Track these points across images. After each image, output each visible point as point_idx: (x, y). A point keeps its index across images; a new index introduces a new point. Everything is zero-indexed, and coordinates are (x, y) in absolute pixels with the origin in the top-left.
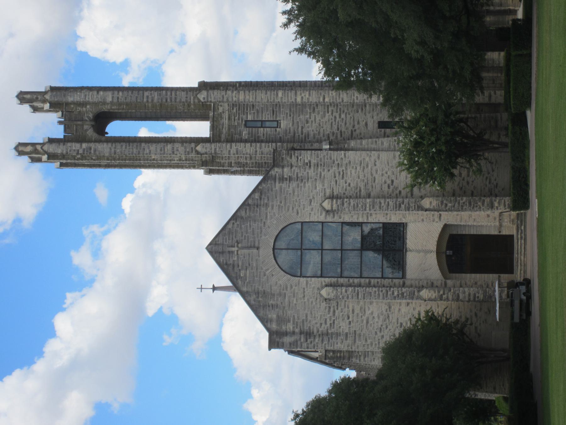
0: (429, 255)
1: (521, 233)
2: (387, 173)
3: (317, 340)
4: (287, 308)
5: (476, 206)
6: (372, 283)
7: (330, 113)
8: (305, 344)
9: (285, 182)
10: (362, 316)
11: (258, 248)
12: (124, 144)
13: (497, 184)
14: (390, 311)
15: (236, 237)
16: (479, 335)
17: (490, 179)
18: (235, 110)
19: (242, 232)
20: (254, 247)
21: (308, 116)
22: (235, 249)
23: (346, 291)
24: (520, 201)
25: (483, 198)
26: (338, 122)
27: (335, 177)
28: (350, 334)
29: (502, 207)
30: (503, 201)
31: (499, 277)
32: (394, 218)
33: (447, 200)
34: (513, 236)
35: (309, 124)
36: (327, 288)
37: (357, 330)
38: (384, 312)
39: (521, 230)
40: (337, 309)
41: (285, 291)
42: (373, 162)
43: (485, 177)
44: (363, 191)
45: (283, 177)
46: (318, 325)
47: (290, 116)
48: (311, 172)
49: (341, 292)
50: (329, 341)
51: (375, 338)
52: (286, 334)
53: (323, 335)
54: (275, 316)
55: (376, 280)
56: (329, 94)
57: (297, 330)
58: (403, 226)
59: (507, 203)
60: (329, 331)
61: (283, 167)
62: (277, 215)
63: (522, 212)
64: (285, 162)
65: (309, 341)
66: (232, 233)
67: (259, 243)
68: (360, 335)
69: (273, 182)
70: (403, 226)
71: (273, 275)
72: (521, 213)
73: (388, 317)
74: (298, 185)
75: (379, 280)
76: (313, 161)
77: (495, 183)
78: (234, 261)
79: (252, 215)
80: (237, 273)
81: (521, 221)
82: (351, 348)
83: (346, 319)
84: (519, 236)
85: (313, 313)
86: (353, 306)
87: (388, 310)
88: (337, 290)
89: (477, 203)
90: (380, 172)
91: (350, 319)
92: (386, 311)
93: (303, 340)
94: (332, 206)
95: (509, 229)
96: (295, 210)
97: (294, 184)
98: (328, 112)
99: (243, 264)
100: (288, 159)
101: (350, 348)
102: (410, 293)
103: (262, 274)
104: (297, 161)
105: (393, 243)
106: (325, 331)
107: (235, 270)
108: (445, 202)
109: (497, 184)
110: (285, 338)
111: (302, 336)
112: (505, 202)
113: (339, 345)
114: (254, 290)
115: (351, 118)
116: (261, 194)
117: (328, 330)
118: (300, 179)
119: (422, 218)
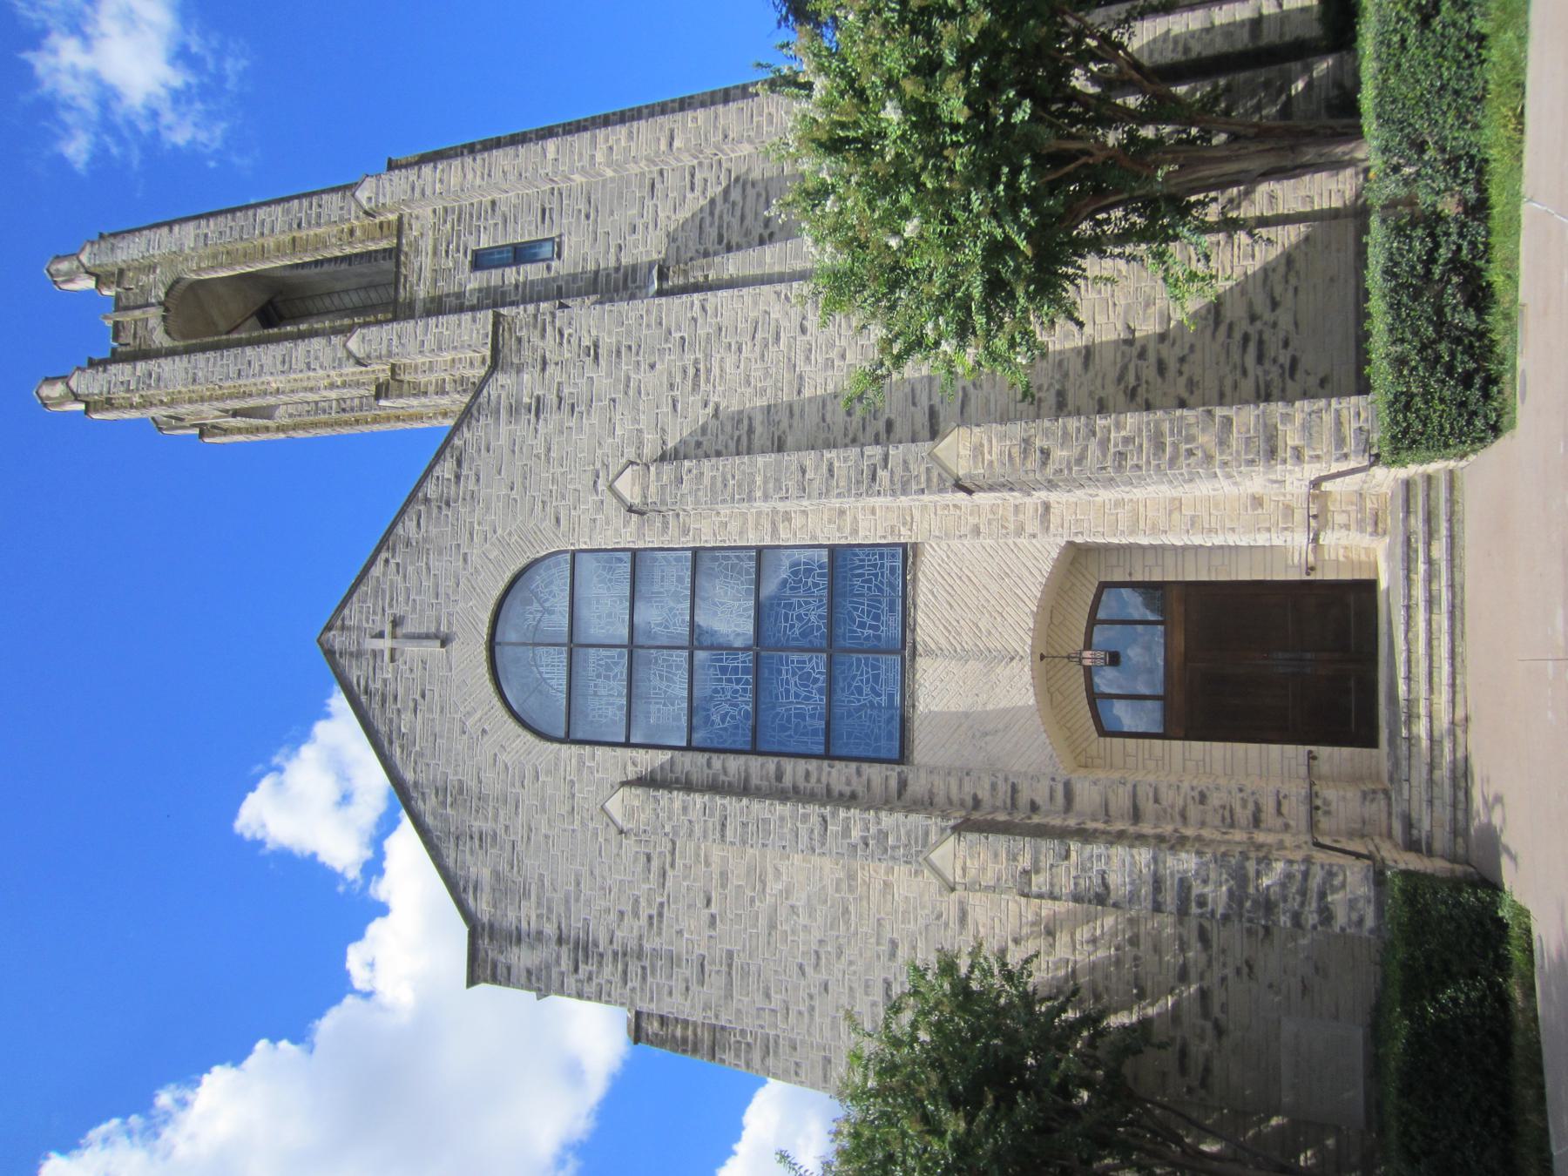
0: (1003, 672)
1: (1430, 577)
2: (843, 357)
3: (607, 970)
4: (520, 847)
5: (1190, 453)
6: (787, 781)
7: (698, 189)
8: (572, 980)
9: (524, 417)
10: (752, 900)
11: (445, 642)
12: (210, 354)
13: (1294, 362)
14: (851, 889)
15: (391, 606)
16: (1220, 1031)
17: (1261, 343)
18: (449, 226)
19: (408, 589)
20: (436, 637)
21: (635, 211)
22: (385, 644)
23: (685, 809)
24: (1455, 385)
25: (1219, 412)
26: (721, 217)
27: (672, 386)
28: (713, 962)
29: (1325, 444)
30: (1328, 418)
31: (1312, 757)
32: (869, 520)
33: (1047, 433)
34: (1370, 586)
35: (639, 236)
36: (626, 791)
37: (736, 948)
38: (830, 890)
39: (1430, 561)
40: (672, 865)
41: (517, 790)
42: (796, 320)
43: (1237, 336)
44: (759, 429)
45: (519, 402)
46: (613, 916)
47: (588, 217)
48: (602, 378)
49: (671, 811)
50: (644, 978)
51: (796, 988)
52: (517, 938)
53: (625, 954)
54: (486, 874)
55: (802, 764)
56: (684, 125)
57: (550, 929)
58: (907, 554)
59: (1349, 430)
60: (647, 946)
61: (519, 370)
62: (499, 531)
63: (1433, 467)
64: (526, 353)
65: (582, 974)
66: (384, 591)
67: (450, 623)
68: (745, 973)
69: (490, 421)
70: (907, 554)
71: (484, 731)
72: (1429, 478)
73: (846, 911)
74: (562, 422)
75: (813, 765)
76: (607, 341)
77: (1284, 358)
78: (385, 681)
79: (434, 531)
80: (391, 721)
81: (1158, 352)
82: (717, 1017)
83: (700, 902)
84: (1419, 593)
85: (597, 872)
86: (724, 859)
87: (844, 886)
88: (657, 800)
89: (1190, 439)
90: (819, 357)
91: (714, 909)
92: (838, 890)
93: (566, 964)
94: (645, 488)
95: (1351, 549)
96: (550, 510)
97: (551, 421)
98: (692, 189)
99: (407, 690)
100: (536, 340)
101: (711, 1014)
102: (908, 834)
103: (457, 728)
104: (561, 344)
105: (869, 622)
106: (632, 944)
107: (389, 715)
108: (1038, 442)
109: (1294, 362)
110: (515, 949)
111: (564, 950)
112: (1339, 423)
113: (678, 997)
114: (434, 781)
115: (759, 195)
116: (459, 463)
117: (640, 937)
118: (566, 407)
119: (972, 520)
